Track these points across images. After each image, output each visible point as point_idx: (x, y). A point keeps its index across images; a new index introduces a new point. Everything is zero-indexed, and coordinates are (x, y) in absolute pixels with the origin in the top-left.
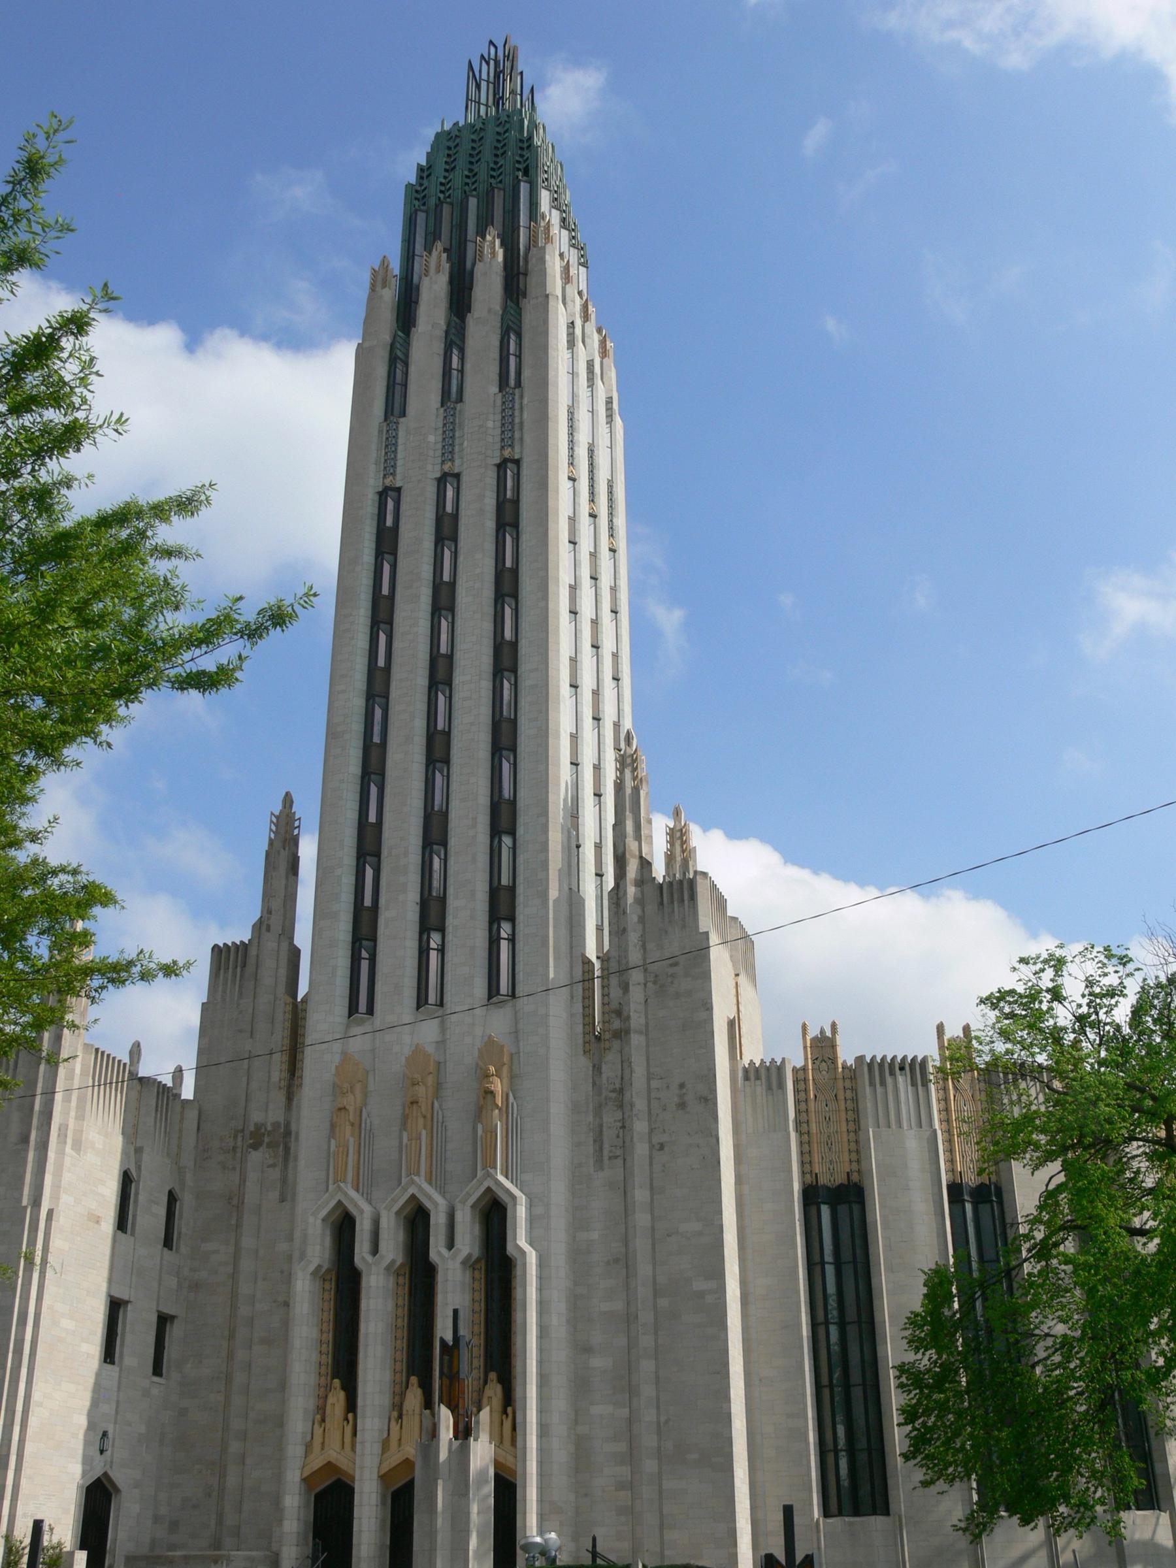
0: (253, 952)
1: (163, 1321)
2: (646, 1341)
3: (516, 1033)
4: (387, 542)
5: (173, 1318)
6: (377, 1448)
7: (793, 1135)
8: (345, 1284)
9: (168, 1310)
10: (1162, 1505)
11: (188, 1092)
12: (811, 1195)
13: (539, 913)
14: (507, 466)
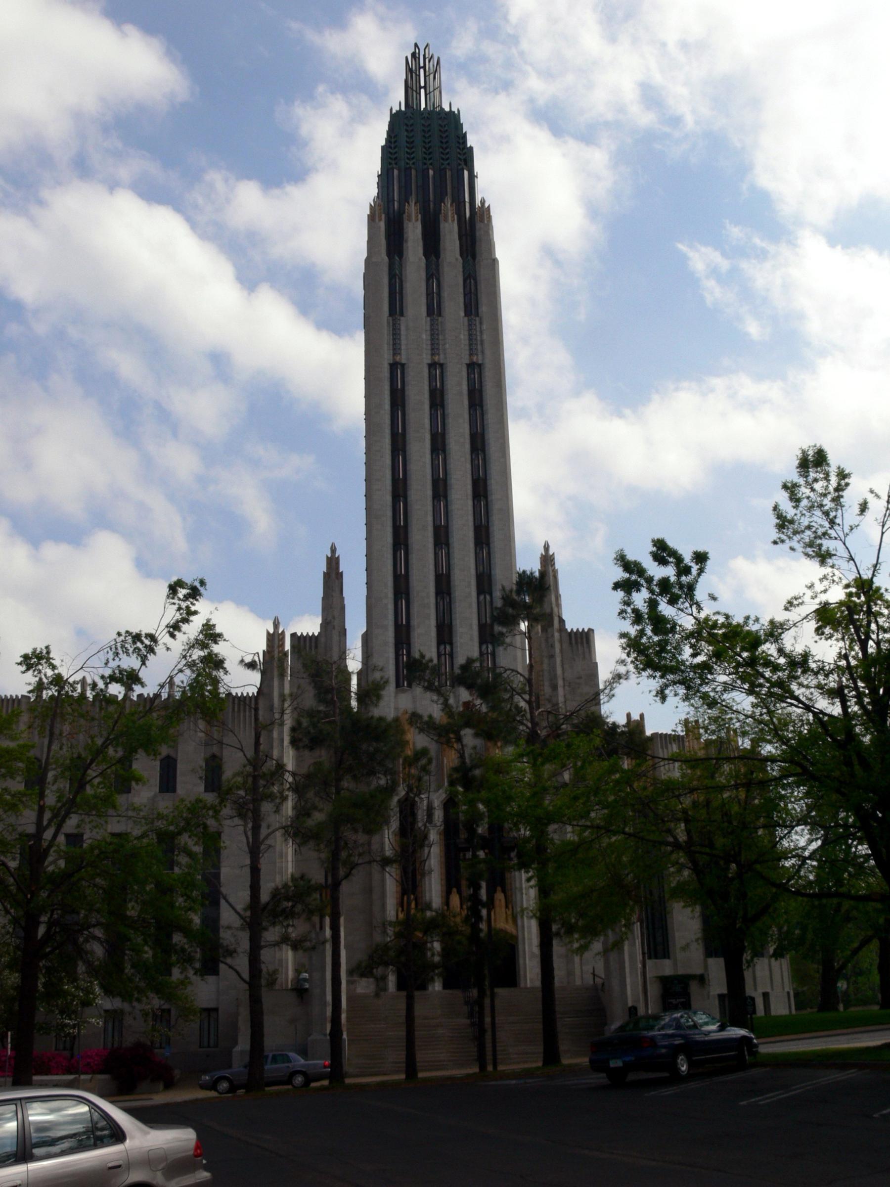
0: (323, 640)
4: (398, 399)
10: (695, 1004)
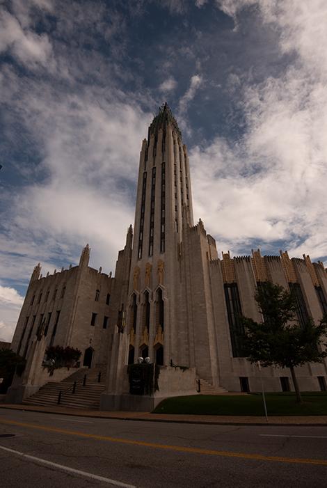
1: (106, 319)
2: (190, 317)
3: (165, 258)
5: (96, 314)
6: (139, 341)
7: (207, 295)
8: (161, 321)
9: (107, 316)
11: (113, 276)
12: (226, 286)
13: (170, 223)
14: (163, 164)
